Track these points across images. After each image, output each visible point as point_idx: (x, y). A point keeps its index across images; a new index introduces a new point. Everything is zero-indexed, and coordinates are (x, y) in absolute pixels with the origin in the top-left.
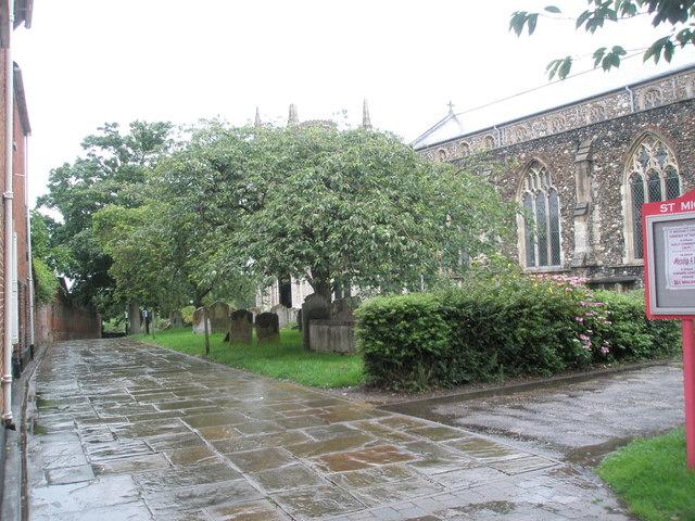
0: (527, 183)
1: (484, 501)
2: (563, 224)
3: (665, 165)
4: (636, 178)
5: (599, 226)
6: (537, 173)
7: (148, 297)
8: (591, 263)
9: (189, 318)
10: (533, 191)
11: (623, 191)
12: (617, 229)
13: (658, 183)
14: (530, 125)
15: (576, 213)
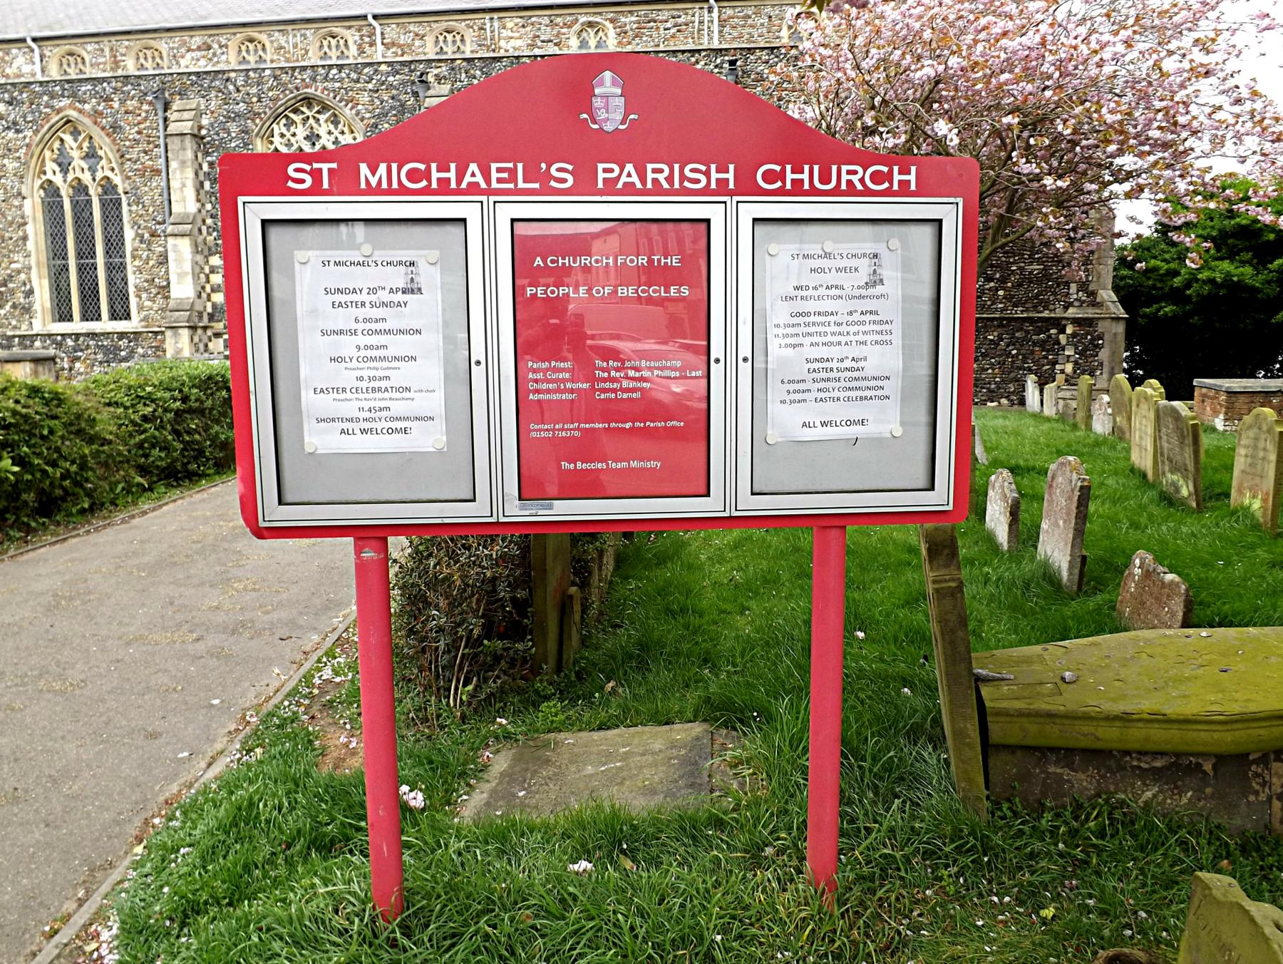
3: (99, 175)
4: (51, 190)
11: (28, 209)
12: (19, 272)
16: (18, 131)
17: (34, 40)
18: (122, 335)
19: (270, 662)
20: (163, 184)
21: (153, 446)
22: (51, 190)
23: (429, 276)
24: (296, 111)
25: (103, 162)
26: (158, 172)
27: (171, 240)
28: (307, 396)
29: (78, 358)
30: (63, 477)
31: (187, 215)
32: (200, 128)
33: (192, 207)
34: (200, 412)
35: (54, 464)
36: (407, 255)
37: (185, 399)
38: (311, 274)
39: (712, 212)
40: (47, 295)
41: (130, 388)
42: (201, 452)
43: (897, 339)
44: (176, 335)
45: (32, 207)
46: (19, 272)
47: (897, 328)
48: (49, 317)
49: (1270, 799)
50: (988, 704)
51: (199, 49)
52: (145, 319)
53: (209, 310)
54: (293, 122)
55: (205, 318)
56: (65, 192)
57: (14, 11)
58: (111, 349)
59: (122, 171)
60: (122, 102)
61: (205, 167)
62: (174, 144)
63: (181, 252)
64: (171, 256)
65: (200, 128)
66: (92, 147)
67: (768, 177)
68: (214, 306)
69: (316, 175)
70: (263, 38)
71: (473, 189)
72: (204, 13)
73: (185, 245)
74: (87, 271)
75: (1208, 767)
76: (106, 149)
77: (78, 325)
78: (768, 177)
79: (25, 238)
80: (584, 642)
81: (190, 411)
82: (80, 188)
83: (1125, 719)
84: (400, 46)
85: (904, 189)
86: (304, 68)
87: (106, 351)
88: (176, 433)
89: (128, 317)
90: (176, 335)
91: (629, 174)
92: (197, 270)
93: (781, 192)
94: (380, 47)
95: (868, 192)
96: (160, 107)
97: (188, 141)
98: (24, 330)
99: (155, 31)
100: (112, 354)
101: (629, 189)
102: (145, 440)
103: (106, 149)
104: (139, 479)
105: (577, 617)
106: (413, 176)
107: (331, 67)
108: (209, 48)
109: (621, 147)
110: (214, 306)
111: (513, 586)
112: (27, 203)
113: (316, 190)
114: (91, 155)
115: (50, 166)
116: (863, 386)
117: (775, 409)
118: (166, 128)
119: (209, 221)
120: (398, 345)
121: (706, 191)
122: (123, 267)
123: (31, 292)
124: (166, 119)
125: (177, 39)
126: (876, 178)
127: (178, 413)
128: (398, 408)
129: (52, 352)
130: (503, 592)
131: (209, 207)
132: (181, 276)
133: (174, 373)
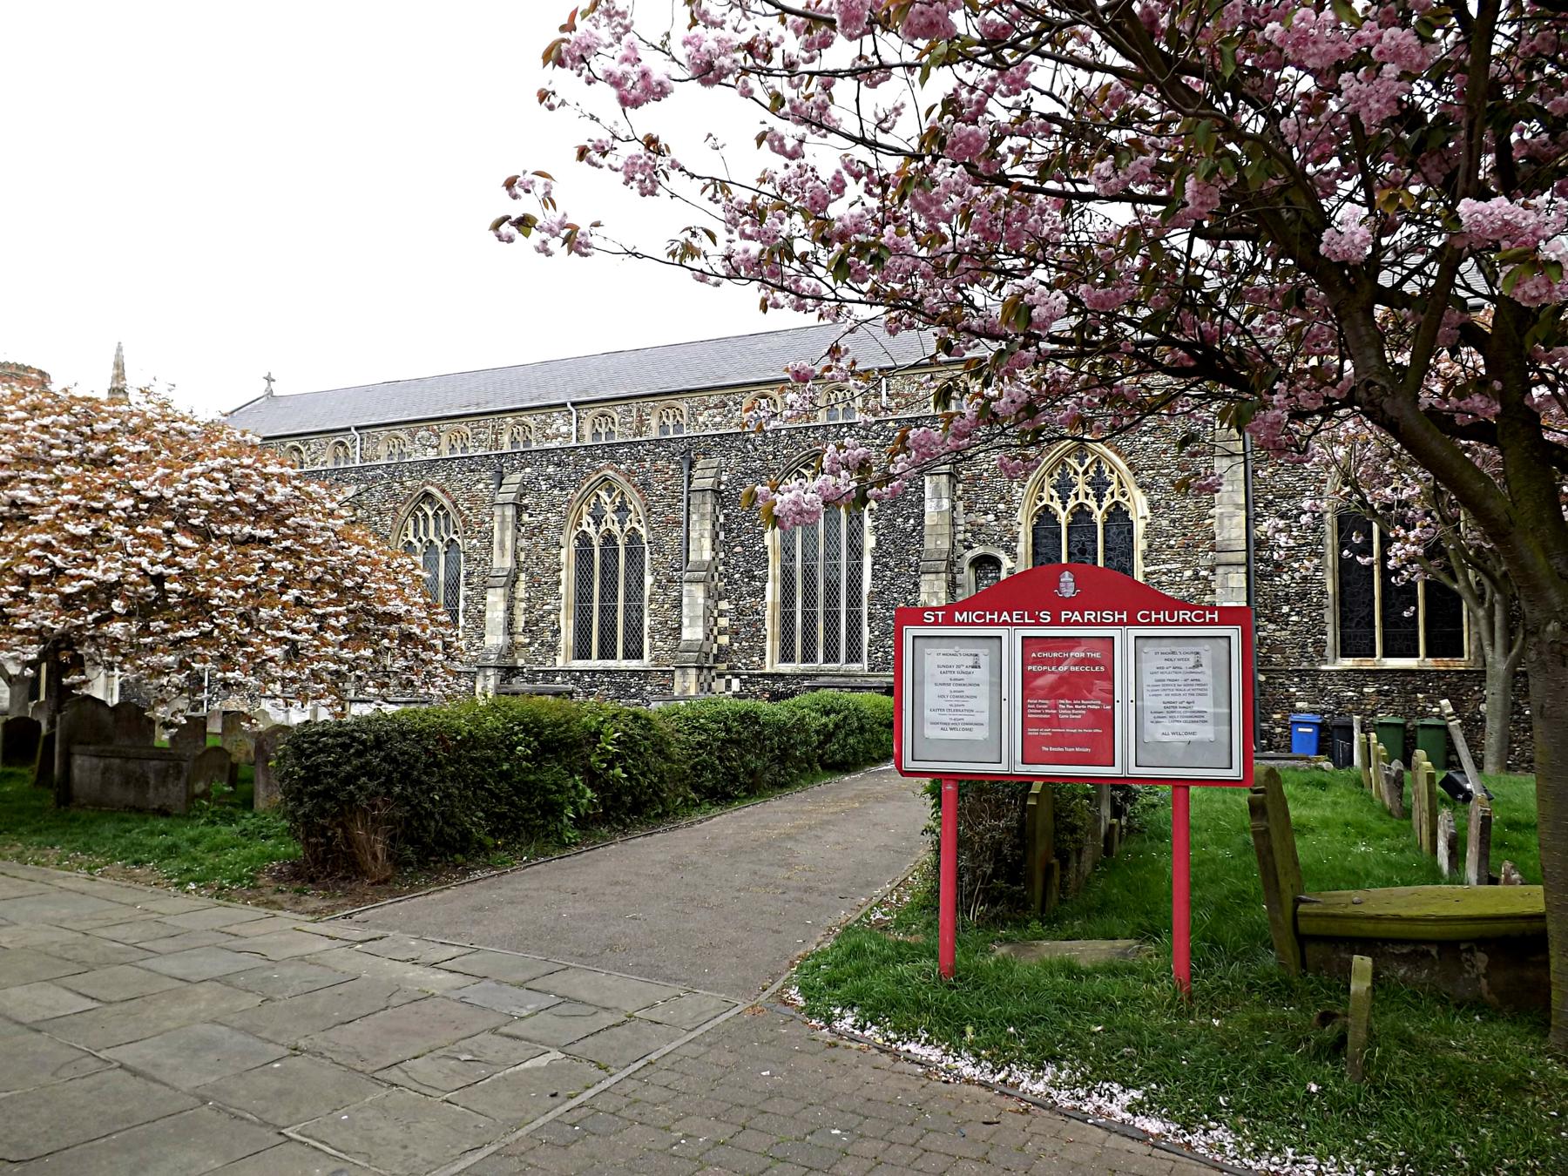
0: (411, 529)
1: (216, 974)
2: (466, 598)
3: (627, 526)
4: (584, 540)
5: (523, 605)
6: (430, 513)
7: (1416, 690)
8: (509, 661)
9: (854, 189)
10: (420, 540)
11: (563, 558)
12: (550, 613)
13: (616, 551)
14: (412, 435)
15: (492, 581)
16: (562, 489)
17: (573, 404)
18: (634, 673)
19: (837, 909)
20: (683, 534)
21: (704, 768)
22: (584, 540)
23: (984, 661)
24: (807, 466)
25: (632, 515)
26: (679, 523)
27: (686, 587)
28: (927, 713)
29: (592, 694)
30: (649, 786)
31: (703, 563)
32: (720, 483)
33: (707, 555)
34: (737, 743)
35: (643, 774)
36: (974, 651)
37: (728, 730)
38: (934, 660)
39: (1114, 632)
40: (571, 635)
41: (687, 719)
42: (736, 777)
43: (1210, 692)
44: (684, 674)
45: (567, 556)
46: (550, 613)
47: (1210, 687)
48: (570, 655)
49: (1478, 978)
50: (1192, 821)
51: (716, 407)
52: (656, 658)
53: (715, 651)
54: (804, 476)
55: (711, 658)
56: (596, 542)
57: (554, 378)
58: (622, 684)
59: (648, 523)
60: (653, 462)
61: (722, 519)
62: (696, 499)
63: (695, 597)
64: (685, 600)
65: (720, 483)
66: (623, 503)
67: (1143, 617)
68: (720, 647)
69: (936, 617)
70: (775, 394)
71: (1005, 623)
72: (721, 373)
73: (699, 592)
74: (608, 612)
75: (1434, 952)
76: (636, 504)
77: (595, 663)
78: (1143, 617)
79: (558, 583)
80: (1061, 901)
81: (731, 741)
82: (609, 539)
83: (1377, 918)
84: (904, 396)
85: (1212, 622)
86: (817, 428)
87: (619, 687)
88: (719, 758)
89: (640, 656)
90: (684, 674)
91: (1076, 616)
92: (710, 616)
93: (1149, 624)
94: (884, 398)
95: (1193, 624)
96: (685, 466)
97: (709, 497)
98: (548, 666)
99: (678, 392)
100: (623, 690)
101: (1076, 623)
102: (697, 763)
103: (636, 504)
104: (693, 795)
105: (1057, 881)
106: (978, 617)
107: (842, 426)
108: (725, 405)
109: (1070, 604)
110: (720, 647)
111: (1014, 847)
112: (563, 551)
113: (936, 623)
114: (622, 509)
115: (586, 518)
116: (1198, 718)
117: (1148, 724)
118: (690, 483)
119: (721, 568)
120: (968, 691)
121: (1113, 624)
122: (640, 609)
123: (559, 631)
124: (690, 476)
125: (696, 399)
126: (1197, 616)
127: (724, 741)
128: (967, 719)
129: (570, 686)
130: (1006, 850)
131: (722, 555)
132: (692, 619)
133: (719, 707)
